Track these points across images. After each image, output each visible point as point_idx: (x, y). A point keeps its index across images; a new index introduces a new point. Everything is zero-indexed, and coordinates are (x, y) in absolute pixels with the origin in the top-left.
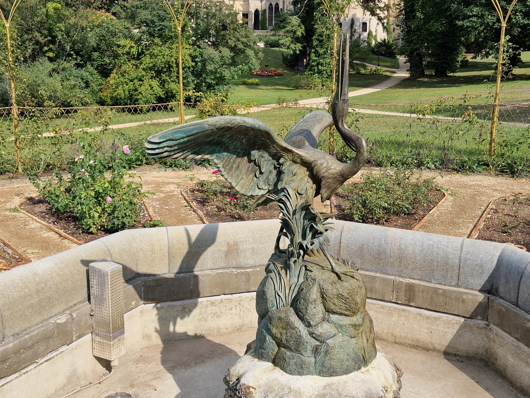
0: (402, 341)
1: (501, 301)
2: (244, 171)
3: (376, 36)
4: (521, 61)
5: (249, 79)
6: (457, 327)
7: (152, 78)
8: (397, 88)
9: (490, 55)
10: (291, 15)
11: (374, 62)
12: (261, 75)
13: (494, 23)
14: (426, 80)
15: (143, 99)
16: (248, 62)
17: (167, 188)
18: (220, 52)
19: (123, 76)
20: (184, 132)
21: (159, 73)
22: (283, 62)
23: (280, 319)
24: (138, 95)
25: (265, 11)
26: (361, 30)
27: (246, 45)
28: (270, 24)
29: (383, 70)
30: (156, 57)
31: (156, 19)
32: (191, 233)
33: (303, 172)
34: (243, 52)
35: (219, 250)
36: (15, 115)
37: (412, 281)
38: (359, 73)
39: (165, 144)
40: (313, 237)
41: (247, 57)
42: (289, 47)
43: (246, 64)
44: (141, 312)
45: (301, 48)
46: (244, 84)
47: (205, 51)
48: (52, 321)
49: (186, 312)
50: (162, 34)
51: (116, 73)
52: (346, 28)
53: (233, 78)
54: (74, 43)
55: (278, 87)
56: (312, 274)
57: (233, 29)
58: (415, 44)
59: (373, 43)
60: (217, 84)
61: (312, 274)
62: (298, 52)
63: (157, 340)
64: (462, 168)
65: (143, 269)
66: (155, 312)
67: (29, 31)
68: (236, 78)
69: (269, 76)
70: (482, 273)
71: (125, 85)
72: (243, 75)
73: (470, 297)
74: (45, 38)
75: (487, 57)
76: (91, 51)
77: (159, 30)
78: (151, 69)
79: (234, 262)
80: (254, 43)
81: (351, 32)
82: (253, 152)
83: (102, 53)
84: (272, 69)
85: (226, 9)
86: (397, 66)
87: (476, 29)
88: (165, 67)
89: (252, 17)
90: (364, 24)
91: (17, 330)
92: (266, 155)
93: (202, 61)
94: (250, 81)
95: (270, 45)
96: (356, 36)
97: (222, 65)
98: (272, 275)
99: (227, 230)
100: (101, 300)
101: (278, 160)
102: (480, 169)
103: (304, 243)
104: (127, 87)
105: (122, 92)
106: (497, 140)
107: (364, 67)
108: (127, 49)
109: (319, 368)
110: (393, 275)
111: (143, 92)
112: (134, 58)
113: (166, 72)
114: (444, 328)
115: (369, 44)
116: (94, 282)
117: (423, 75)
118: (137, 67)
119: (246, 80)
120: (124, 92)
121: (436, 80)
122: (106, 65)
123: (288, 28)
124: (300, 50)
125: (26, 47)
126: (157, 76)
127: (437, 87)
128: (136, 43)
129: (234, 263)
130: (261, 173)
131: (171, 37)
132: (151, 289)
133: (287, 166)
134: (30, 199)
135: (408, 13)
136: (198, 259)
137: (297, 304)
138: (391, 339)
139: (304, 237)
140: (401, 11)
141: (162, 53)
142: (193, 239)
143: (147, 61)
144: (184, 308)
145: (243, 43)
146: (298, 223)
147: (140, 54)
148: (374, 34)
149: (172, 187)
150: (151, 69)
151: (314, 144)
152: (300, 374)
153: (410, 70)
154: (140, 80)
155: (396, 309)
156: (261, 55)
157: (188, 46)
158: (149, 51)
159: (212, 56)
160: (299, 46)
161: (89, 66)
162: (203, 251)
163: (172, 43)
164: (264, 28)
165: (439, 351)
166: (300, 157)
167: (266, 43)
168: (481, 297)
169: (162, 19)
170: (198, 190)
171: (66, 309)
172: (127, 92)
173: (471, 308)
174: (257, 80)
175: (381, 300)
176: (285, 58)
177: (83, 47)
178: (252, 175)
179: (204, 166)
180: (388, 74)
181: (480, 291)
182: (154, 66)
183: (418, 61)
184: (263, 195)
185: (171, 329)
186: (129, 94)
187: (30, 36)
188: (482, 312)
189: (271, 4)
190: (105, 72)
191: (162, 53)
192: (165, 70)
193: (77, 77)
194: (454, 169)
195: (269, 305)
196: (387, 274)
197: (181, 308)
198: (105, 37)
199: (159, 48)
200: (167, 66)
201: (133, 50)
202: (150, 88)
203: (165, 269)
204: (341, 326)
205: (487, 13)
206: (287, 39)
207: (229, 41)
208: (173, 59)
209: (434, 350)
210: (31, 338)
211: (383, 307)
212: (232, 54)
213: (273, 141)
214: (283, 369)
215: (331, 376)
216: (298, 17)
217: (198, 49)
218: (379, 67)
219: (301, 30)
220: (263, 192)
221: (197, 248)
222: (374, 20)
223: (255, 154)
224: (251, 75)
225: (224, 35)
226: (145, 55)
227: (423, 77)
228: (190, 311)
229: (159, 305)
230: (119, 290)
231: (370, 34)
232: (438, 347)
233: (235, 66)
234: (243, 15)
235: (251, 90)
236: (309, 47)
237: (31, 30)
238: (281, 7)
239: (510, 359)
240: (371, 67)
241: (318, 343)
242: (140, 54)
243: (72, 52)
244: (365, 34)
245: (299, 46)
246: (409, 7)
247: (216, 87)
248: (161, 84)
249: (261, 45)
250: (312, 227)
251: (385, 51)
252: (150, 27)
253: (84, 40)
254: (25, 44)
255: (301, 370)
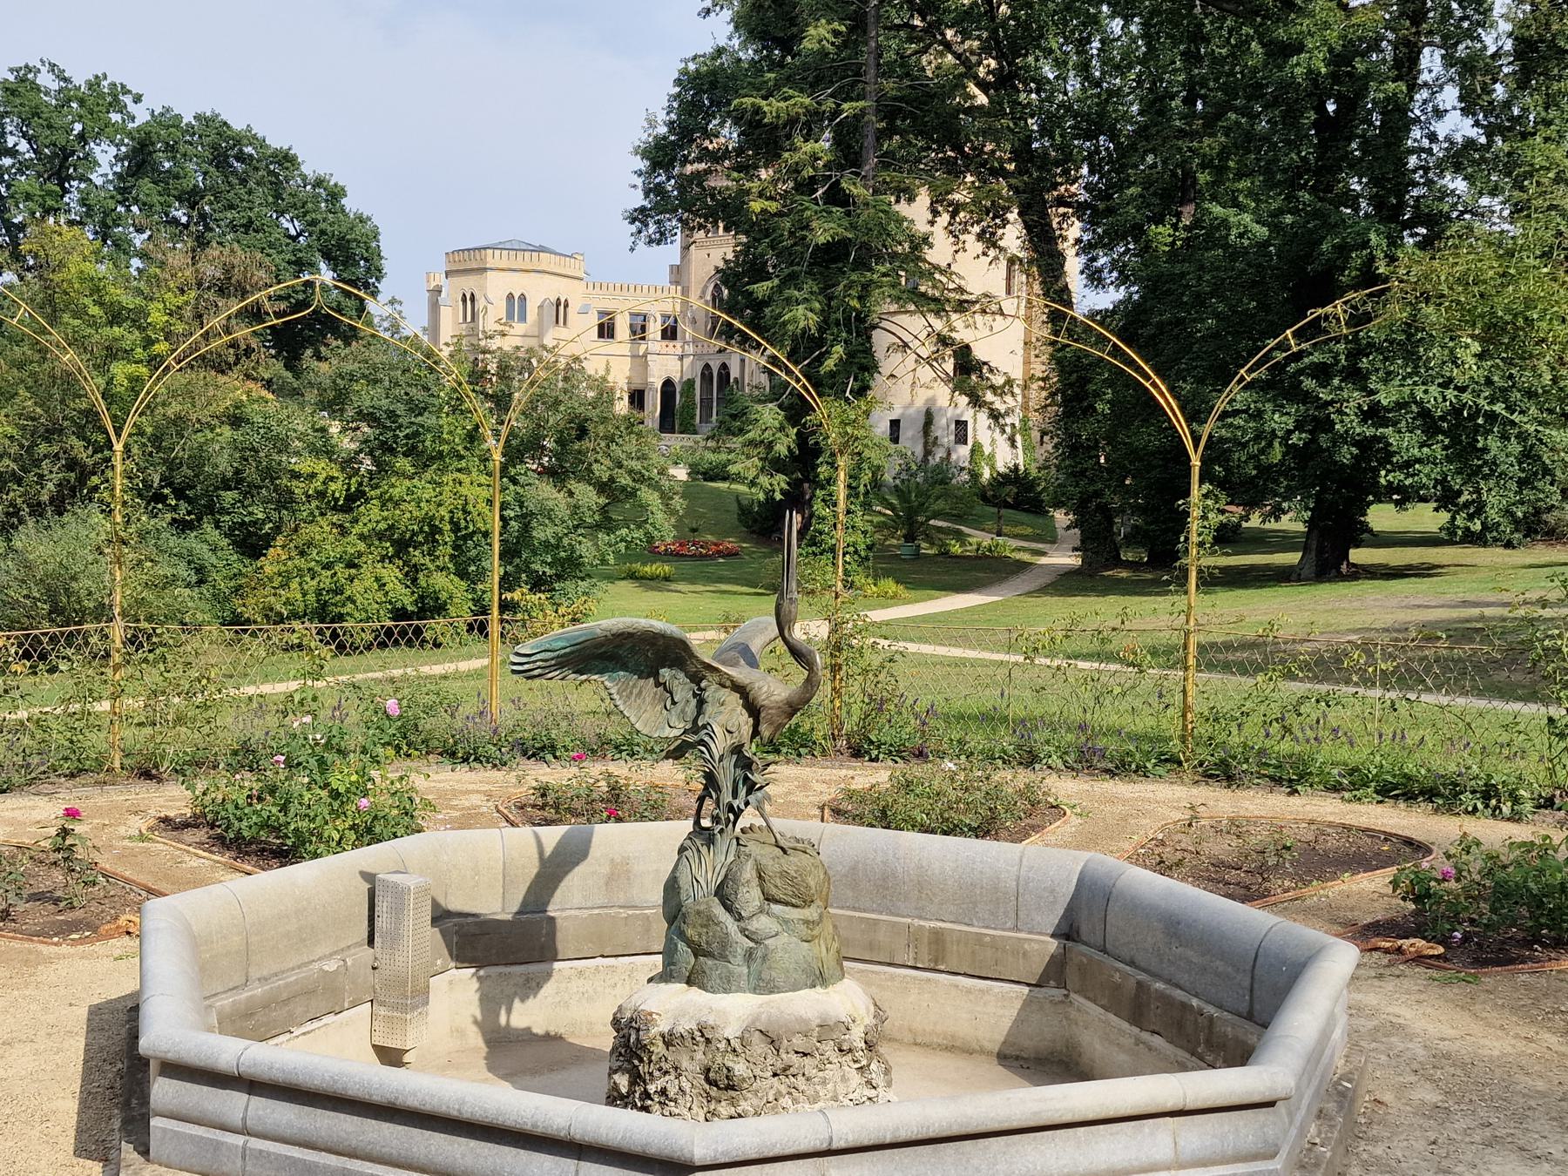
0: (927, 1040)
1: (1083, 948)
2: (648, 700)
3: (992, 457)
4: (1370, 531)
5: (644, 564)
6: (1018, 1005)
7: (382, 561)
8: (1046, 594)
9: (1285, 513)
10: (760, 402)
11: (989, 524)
12: (677, 554)
13: (1289, 432)
14: (1124, 575)
15: (357, 615)
16: (646, 522)
17: (465, 802)
18: (571, 494)
19: (302, 554)
20: (567, 639)
21: (402, 546)
22: (740, 521)
23: (698, 913)
24: (344, 605)
25: (690, 384)
26: (952, 437)
27: (640, 478)
28: (706, 418)
29: (1010, 547)
30: (397, 504)
31: (400, 409)
32: (544, 840)
33: (734, 699)
34: (633, 494)
35: (594, 873)
36: (118, 641)
37: (940, 924)
38: (945, 554)
39: (538, 657)
40: (749, 793)
41: (644, 507)
42: (755, 481)
43: (639, 527)
44: (451, 983)
45: (786, 487)
46: (631, 576)
47: (529, 493)
48: (316, 966)
49: (531, 987)
50: (414, 447)
51: (283, 547)
52: (910, 433)
53: (604, 561)
54: (172, 465)
55: (724, 587)
56: (747, 850)
57: (605, 438)
58: (1092, 481)
59: (986, 474)
60: (559, 577)
61: (747, 850)
62: (778, 496)
63: (476, 1039)
64: (1121, 768)
65: (455, 904)
66: (475, 985)
67: (52, 432)
68: (612, 562)
69: (702, 557)
70: (1054, 903)
71: (308, 579)
72: (631, 553)
73: (1036, 946)
74: (95, 452)
75: (1277, 519)
76: (217, 488)
77: (407, 437)
78: (381, 536)
79: (621, 895)
80: (662, 472)
81: (926, 444)
82: (662, 671)
83: (250, 491)
84: (710, 537)
85: (590, 388)
86: (1049, 537)
87: (1244, 445)
88: (421, 530)
89: (654, 403)
90: (961, 425)
91: (265, 973)
92: (681, 675)
93: (524, 516)
94: (647, 569)
95: (704, 474)
96: (940, 454)
97: (576, 527)
98: (688, 853)
99: (608, 837)
100: (395, 939)
101: (698, 684)
102: (1160, 770)
103: (735, 803)
104: (314, 583)
105: (299, 596)
106: (1197, 709)
107: (960, 536)
108: (317, 484)
109: (753, 982)
110: (908, 916)
111: (359, 599)
112: (334, 508)
113: (421, 544)
114: (995, 1009)
115: (975, 476)
116: (382, 907)
117: (1118, 563)
118: (344, 532)
119: (638, 566)
120: (304, 595)
121: (1149, 576)
122: (255, 523)
123: (750, 435)
124: (783, 492)
125: (41, 476)
126: (397, 555)
127: (1149, 594)
128: (343, 470)
129: (621, 898)
130: (674, 703)
131: (441, 455)
132: (470, 940)
133: (712, 692)
134: (166, 820)
135: (1070, 401)
136: (556, 888)
137: (724, 894)
138: (908, 1038)
139: (735, 795)
140: (1052, 395)
141: (416, 495)
142: (548, 851)
143: (372, 515)
144: (527, 980)
145: (631, 472)
146: (727, 774)
147: (354, 498)
148: (987, 450)
149: (476, 799)
150: (381, 536)
151: (753, 663)
152: (726, 991)
153: (1082, 548)
154: (351, 565)
155: (915, 978)
156: (678, 503)
157: (483, 479)
158: (378, 492)
159: (550, 504)
160: (780, 481)
161: (208, 527)
162: (567, 873)
163: (443, 471)
164: (688, 428)
165: (989, 1053)
166: (729, 677)
167: (694, 471)
168: (1053, 945)
169: (418, 409)
170: (534, 806)
171: (335, 953)
172: (311, 598)
173: (1037, 967)
174: (667, 568)
175: (890, 964)
176: (744, 511)
177: (196, 476)
178: (659, 708)
179: (543, 759)
180: (1026, 557)
181: (1053, 936)
182: (391, 527)
183: (1100, 524)
184: (676, 738)
185: (503, 1020)
186: (318, 601)
187: (56, 449)
188: (1055, 973)
189: (707, 366)
190: (251, 544)
191: (416, 495)
192: (420, 538)
193: (179, 555)
194: (1107, 771)
195: (683, 896)
196: (898, 915)
197: (521, 980)
198: (257, 452)
199: (407, 483)
200: (426, 529)
201: (333, 486)
202: (378, 585)
203: (495, 902)
204: (786, 921)
205: (1269, 406)
206: (749, 463)
207: (595, 466)
208: (443, 512)
209: (982, 1051)
210: (287, 985)
211: (892, 978)
212: (603, 501)
213: (692, 655)
214: (703, 987)
215: (771, 992)
216: (780, 407)
217: (512, 487)
218: (1001, 540)
219: (786, 441)
220: (677, 733)
221: (553, 870)
222: (983, 418)
223: (665, 673)
224: (653, 554)
225: (579, 452)
226: (367, 501)
227: (1116, 566)
228: (539, 986)
229: (482, 973)
230: (418, 939)
231: (976, 450)
232: (988, 1046)
233: (610, 530)
234: (632, 398)
235: (650, 593)
236: (809, 481)
237: (61, 431)
238: (734, 373)
239: (1098, 1046)
240: (980, 539)
241: (752, 944)
242: (354, 498)
243: (166, 491)
244: (963, 452)
245: (780, 481)
246: (1071, 385)
247: (556, 586)
248: (406, 575)
249: (681, 473)
250: (746, 779)
251: (1016, 496)
252: (385, 427)
253: (199, 460)
254: (39, 467)
255: (727, 985)
